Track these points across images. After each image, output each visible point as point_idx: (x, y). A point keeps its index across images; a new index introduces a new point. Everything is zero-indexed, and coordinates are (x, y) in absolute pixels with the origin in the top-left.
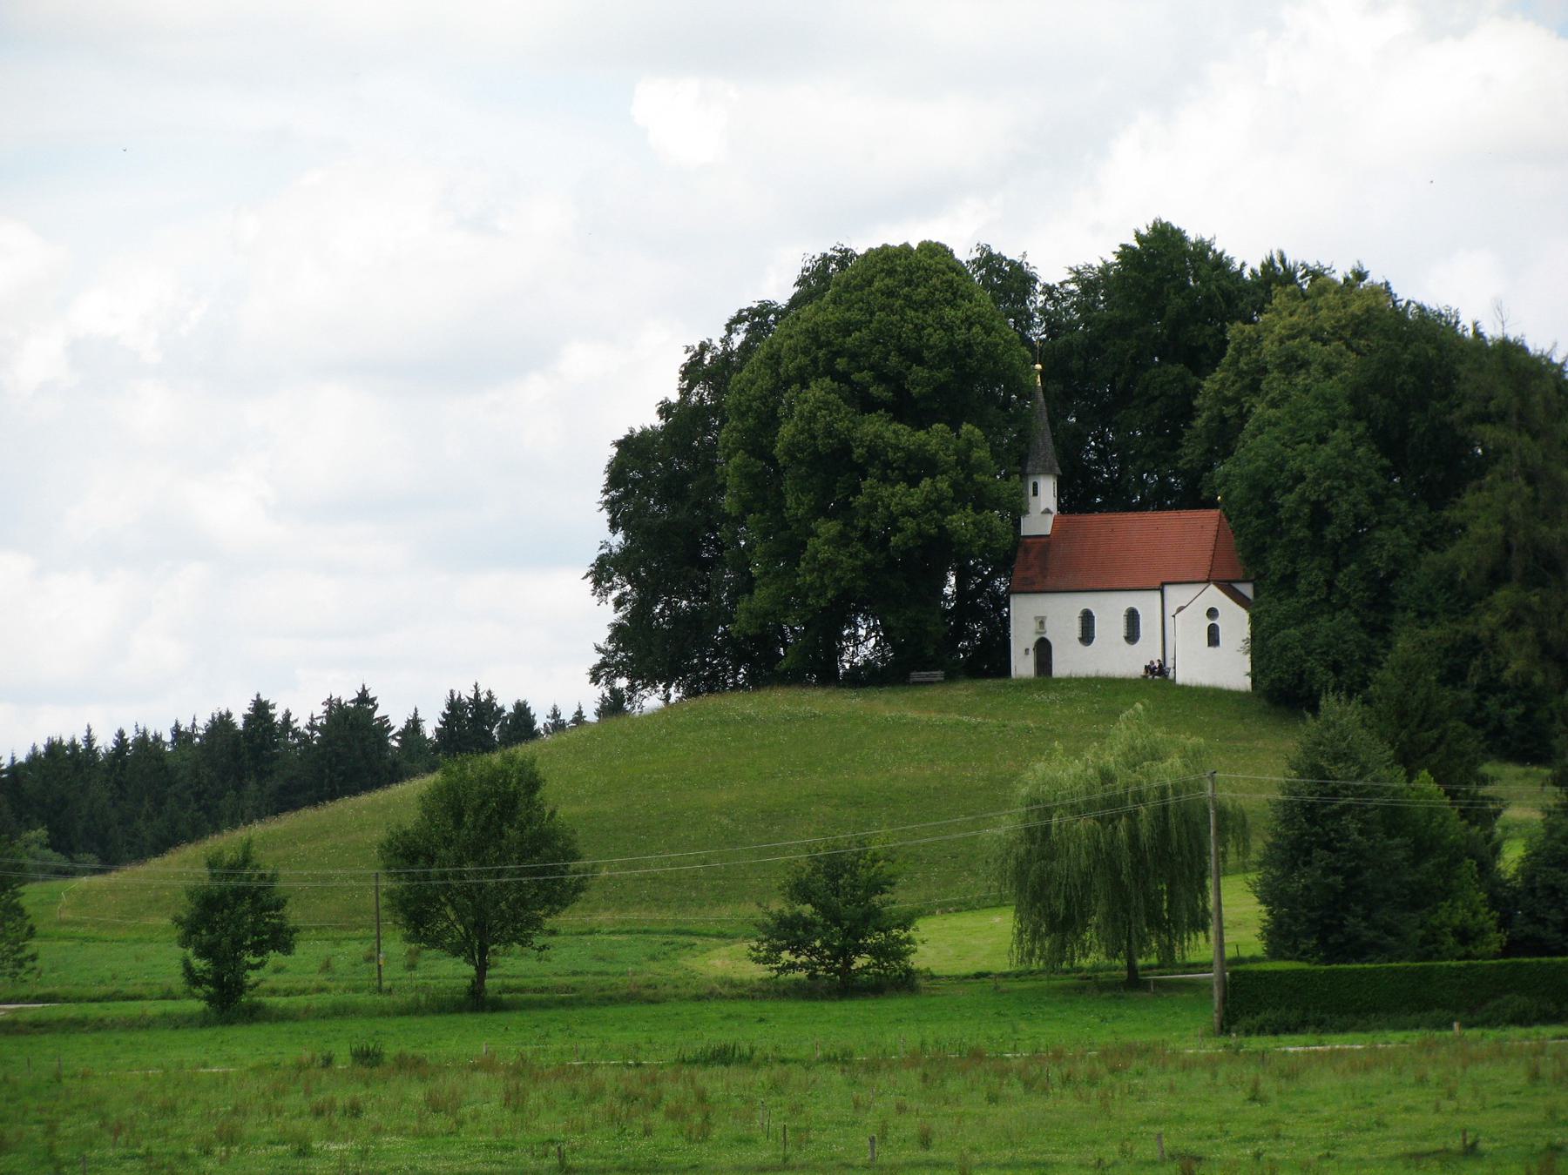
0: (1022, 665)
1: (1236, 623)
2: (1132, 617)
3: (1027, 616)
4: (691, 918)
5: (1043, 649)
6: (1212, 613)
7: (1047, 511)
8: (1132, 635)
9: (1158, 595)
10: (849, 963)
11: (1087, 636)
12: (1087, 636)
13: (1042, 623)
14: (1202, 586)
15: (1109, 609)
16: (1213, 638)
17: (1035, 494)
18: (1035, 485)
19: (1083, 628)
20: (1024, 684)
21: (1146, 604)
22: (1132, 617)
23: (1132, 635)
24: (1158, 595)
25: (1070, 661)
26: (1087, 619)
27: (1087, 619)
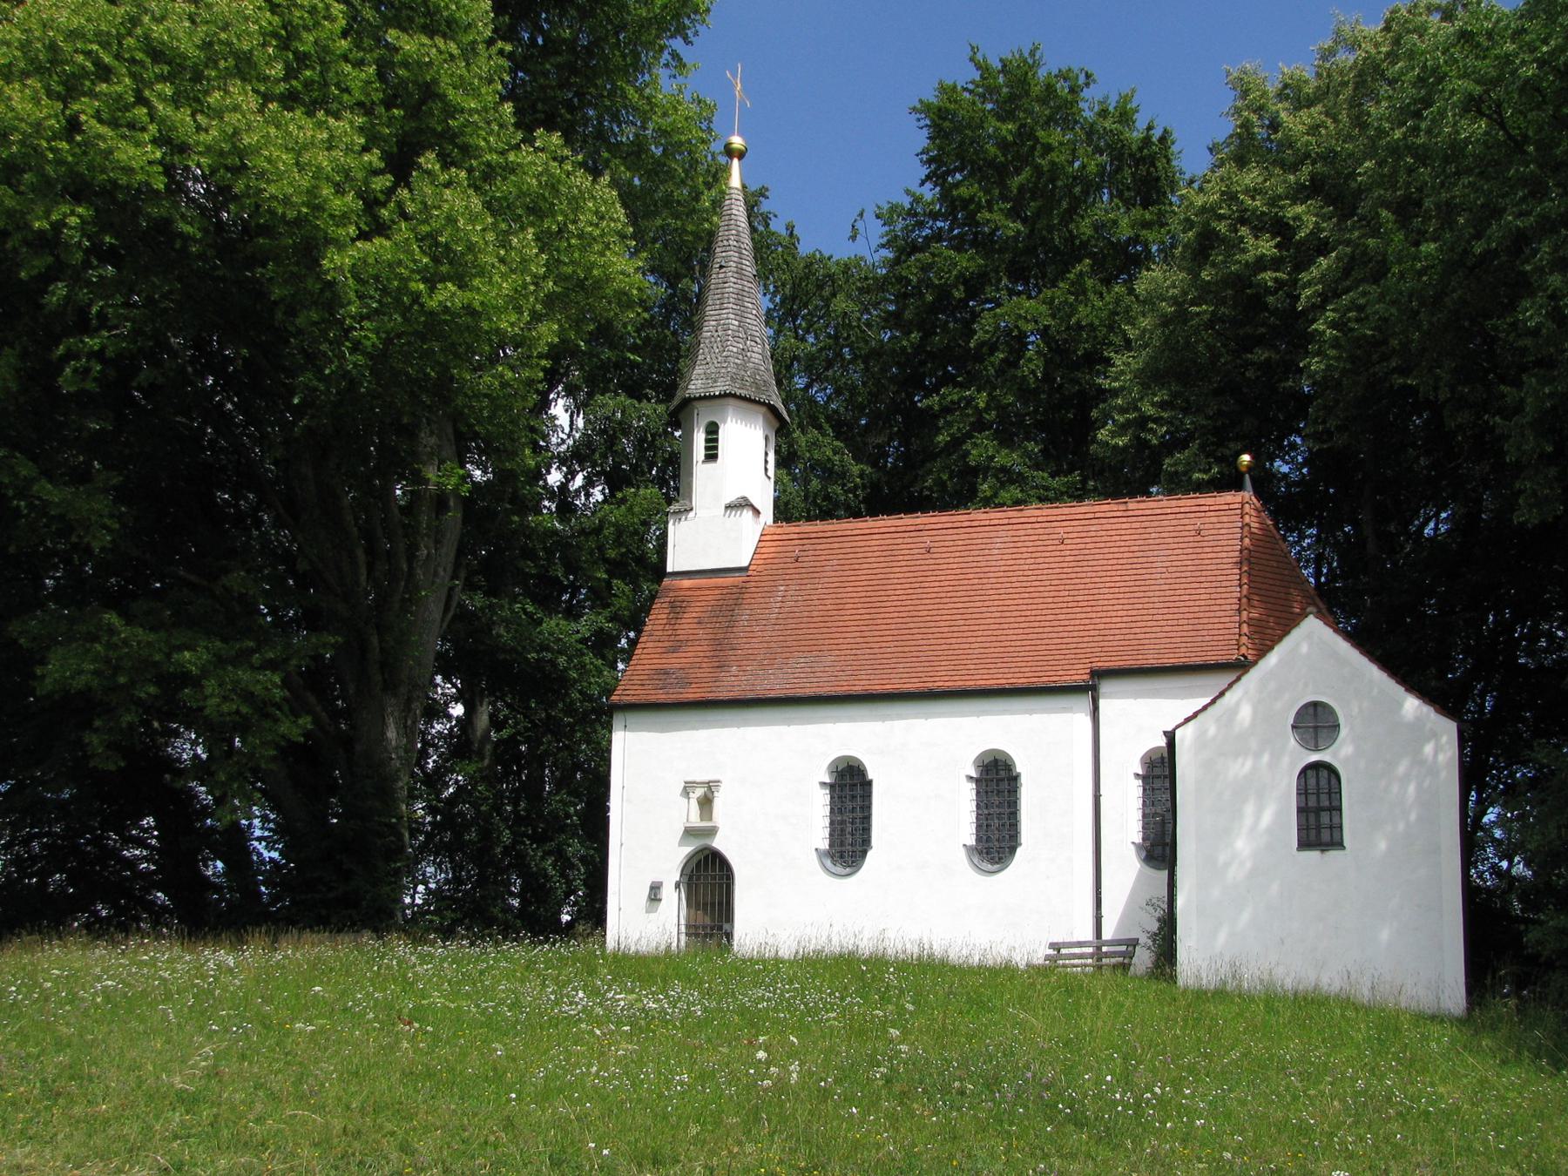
0: (641, 908)
1: (1404, 751)
2: (997, 782)
3: (654, 779)
4: (1318, 600)
5: (709, 880)
6: (1316, 722)
7: (742, 504)
8: (997, 836)
9: (1085, 701)
10: (293, 1020)
11: (849, 840)
12: (849, 840)
13: (706, 803)
14: (1223, 680)
15: (922, 761)
16: (1319, 815)
17: (711, 456)
18: (712, 430)
19: (837, 808)
20: (641, 969)
21: (1043, 740)
22: (997, 782)
23: (997, 836)
24: (1083, 720)
25: (788, 906)
26: (850, 788)
27: (850, 788)
